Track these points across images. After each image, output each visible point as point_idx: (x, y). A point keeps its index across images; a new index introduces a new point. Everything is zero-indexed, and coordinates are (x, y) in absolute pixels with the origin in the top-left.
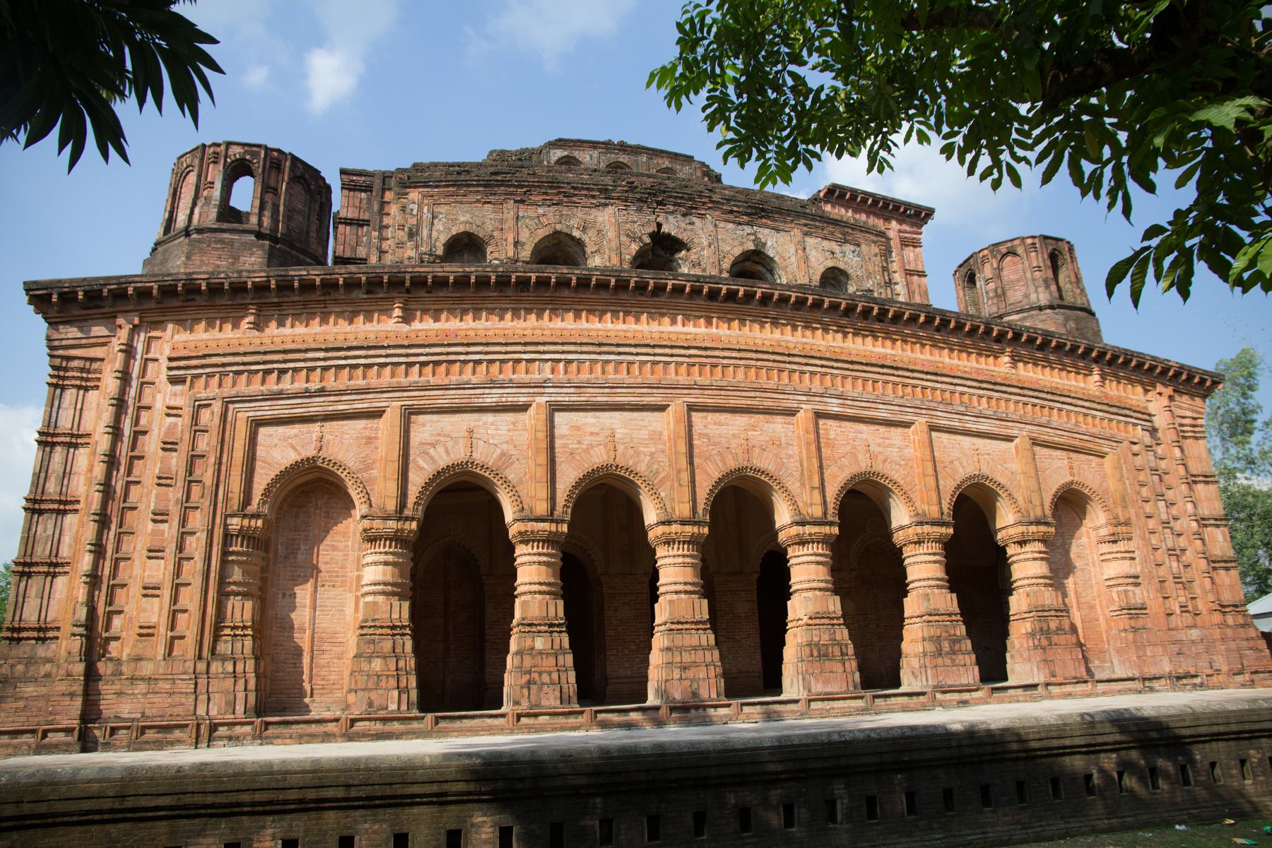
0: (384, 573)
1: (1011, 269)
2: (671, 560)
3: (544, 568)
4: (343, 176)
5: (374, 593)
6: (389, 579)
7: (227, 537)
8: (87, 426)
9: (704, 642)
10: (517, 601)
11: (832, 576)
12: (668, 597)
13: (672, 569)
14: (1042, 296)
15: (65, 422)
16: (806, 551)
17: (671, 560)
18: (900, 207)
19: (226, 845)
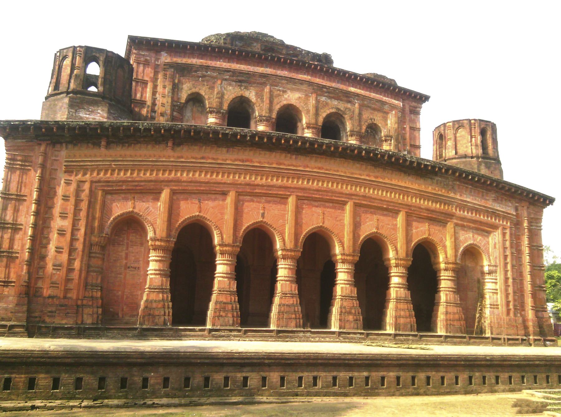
0: (159, 266)
1: (463, 133)
2: (283, 266)
3: (346, 274)
4: (72, 49)
5: (222, 277)
6: (157, 268)
7: (91, 245)
8: (24, 191)
9: (456, 311)
10: (216, 279)
11: (354, 279)
12: (219, 279)
13: (343, 274)
14: (474, 151)
15: (13, 189)
16: (491, 277)
17: (283, 266)
18: (407, 93)
19: (560, 383)
